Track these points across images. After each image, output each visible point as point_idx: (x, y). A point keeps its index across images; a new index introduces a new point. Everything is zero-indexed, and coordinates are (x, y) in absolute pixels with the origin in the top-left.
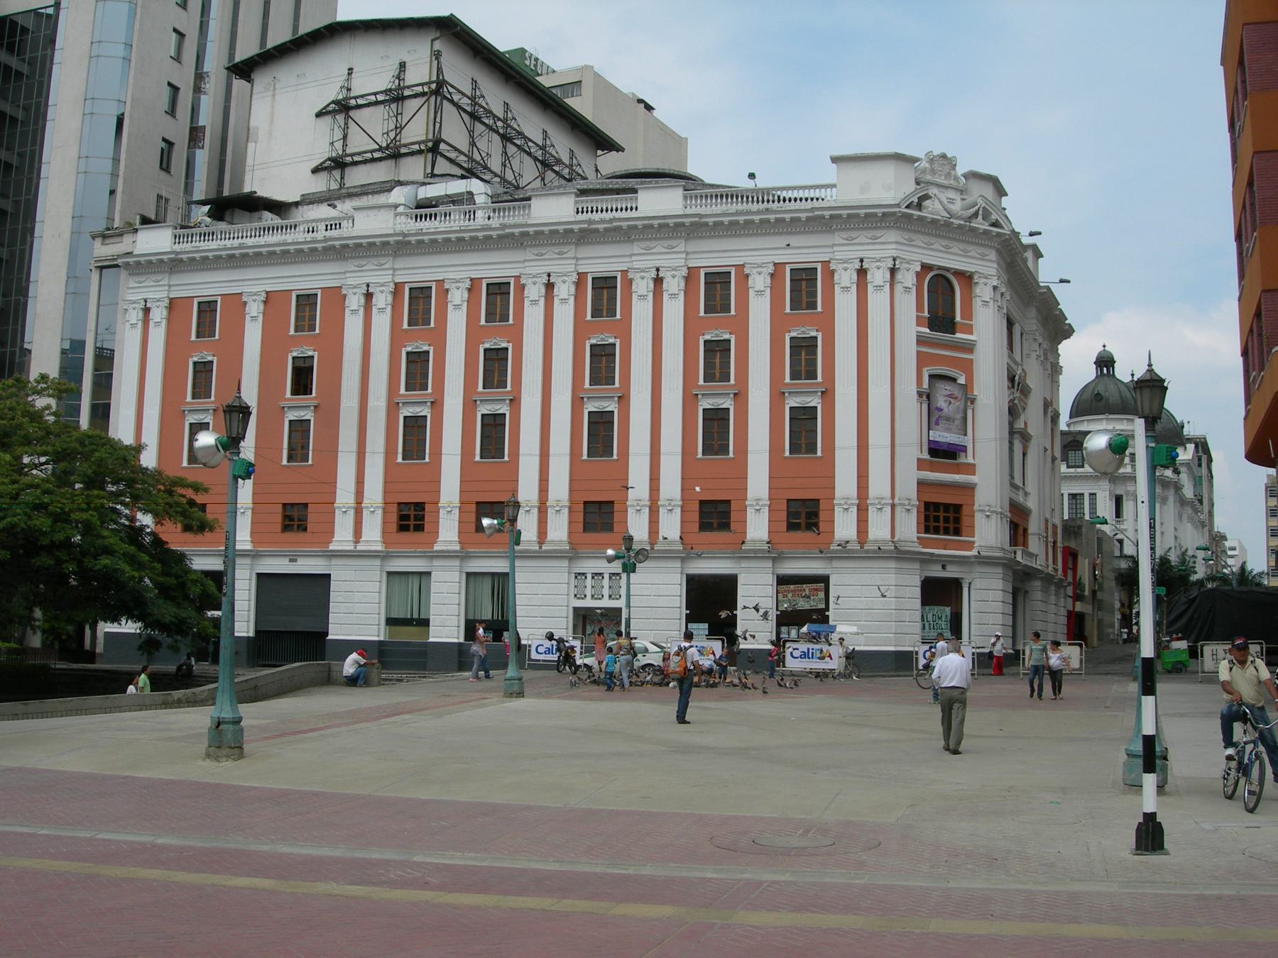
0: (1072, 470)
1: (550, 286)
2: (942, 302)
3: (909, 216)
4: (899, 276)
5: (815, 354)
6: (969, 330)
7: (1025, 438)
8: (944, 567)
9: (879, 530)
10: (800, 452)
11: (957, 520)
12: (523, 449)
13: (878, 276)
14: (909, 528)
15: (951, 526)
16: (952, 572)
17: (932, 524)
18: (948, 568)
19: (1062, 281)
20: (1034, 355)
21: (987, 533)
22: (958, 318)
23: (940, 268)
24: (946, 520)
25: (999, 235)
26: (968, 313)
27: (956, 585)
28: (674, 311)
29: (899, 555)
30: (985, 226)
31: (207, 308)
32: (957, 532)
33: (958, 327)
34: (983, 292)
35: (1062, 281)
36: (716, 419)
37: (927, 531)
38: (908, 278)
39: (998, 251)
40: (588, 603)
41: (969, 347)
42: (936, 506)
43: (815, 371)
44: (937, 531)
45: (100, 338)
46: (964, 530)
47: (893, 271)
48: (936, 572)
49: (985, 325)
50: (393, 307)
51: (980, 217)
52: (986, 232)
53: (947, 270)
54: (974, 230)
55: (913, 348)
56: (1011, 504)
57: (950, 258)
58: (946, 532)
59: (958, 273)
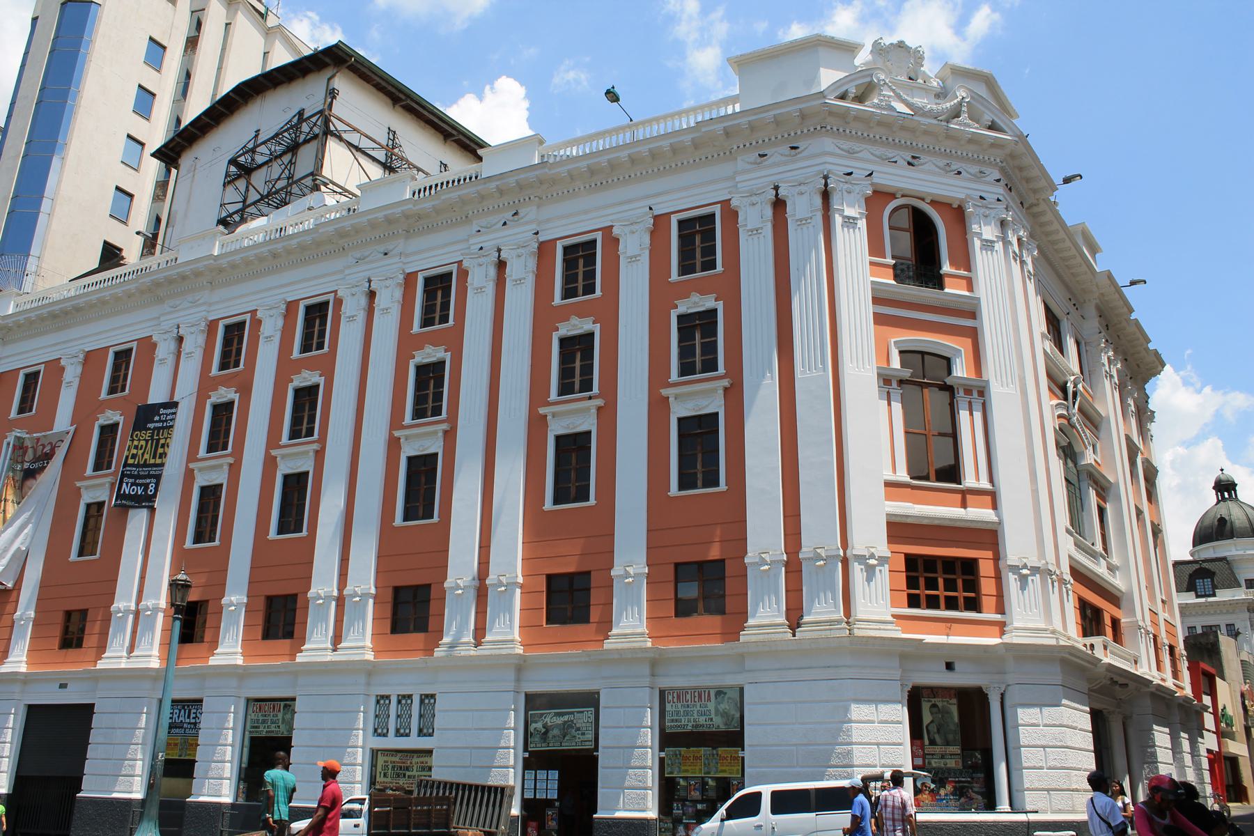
0: (1202, 600)
1: (779, 205)
2: (922, 248)
3: (843, 115)
5: (715, 334)
7: (1104, 490)
8: (949, 666)
10: (694, 486)
13: (802, 206)
17: (923, 592)
19: (1133, 283)
21: (1037, 616)
25: (996, 145)
28: (520, 301)
30: (975, 129)
31: (122, 357)
35: (1133, 283)
36: (573, 448)
37: (913, 602)
40: (392, 742)
42: (930, 563)
43: (716, 359)
44: (933, 603)
45: (667, 770)
47: (826, 195)
50: (537, 276)
51: (964, 116)
52: (974, 140)
54: (950, 136)
55: (867, 309)
57: (928, 182)
58: (952, 604)
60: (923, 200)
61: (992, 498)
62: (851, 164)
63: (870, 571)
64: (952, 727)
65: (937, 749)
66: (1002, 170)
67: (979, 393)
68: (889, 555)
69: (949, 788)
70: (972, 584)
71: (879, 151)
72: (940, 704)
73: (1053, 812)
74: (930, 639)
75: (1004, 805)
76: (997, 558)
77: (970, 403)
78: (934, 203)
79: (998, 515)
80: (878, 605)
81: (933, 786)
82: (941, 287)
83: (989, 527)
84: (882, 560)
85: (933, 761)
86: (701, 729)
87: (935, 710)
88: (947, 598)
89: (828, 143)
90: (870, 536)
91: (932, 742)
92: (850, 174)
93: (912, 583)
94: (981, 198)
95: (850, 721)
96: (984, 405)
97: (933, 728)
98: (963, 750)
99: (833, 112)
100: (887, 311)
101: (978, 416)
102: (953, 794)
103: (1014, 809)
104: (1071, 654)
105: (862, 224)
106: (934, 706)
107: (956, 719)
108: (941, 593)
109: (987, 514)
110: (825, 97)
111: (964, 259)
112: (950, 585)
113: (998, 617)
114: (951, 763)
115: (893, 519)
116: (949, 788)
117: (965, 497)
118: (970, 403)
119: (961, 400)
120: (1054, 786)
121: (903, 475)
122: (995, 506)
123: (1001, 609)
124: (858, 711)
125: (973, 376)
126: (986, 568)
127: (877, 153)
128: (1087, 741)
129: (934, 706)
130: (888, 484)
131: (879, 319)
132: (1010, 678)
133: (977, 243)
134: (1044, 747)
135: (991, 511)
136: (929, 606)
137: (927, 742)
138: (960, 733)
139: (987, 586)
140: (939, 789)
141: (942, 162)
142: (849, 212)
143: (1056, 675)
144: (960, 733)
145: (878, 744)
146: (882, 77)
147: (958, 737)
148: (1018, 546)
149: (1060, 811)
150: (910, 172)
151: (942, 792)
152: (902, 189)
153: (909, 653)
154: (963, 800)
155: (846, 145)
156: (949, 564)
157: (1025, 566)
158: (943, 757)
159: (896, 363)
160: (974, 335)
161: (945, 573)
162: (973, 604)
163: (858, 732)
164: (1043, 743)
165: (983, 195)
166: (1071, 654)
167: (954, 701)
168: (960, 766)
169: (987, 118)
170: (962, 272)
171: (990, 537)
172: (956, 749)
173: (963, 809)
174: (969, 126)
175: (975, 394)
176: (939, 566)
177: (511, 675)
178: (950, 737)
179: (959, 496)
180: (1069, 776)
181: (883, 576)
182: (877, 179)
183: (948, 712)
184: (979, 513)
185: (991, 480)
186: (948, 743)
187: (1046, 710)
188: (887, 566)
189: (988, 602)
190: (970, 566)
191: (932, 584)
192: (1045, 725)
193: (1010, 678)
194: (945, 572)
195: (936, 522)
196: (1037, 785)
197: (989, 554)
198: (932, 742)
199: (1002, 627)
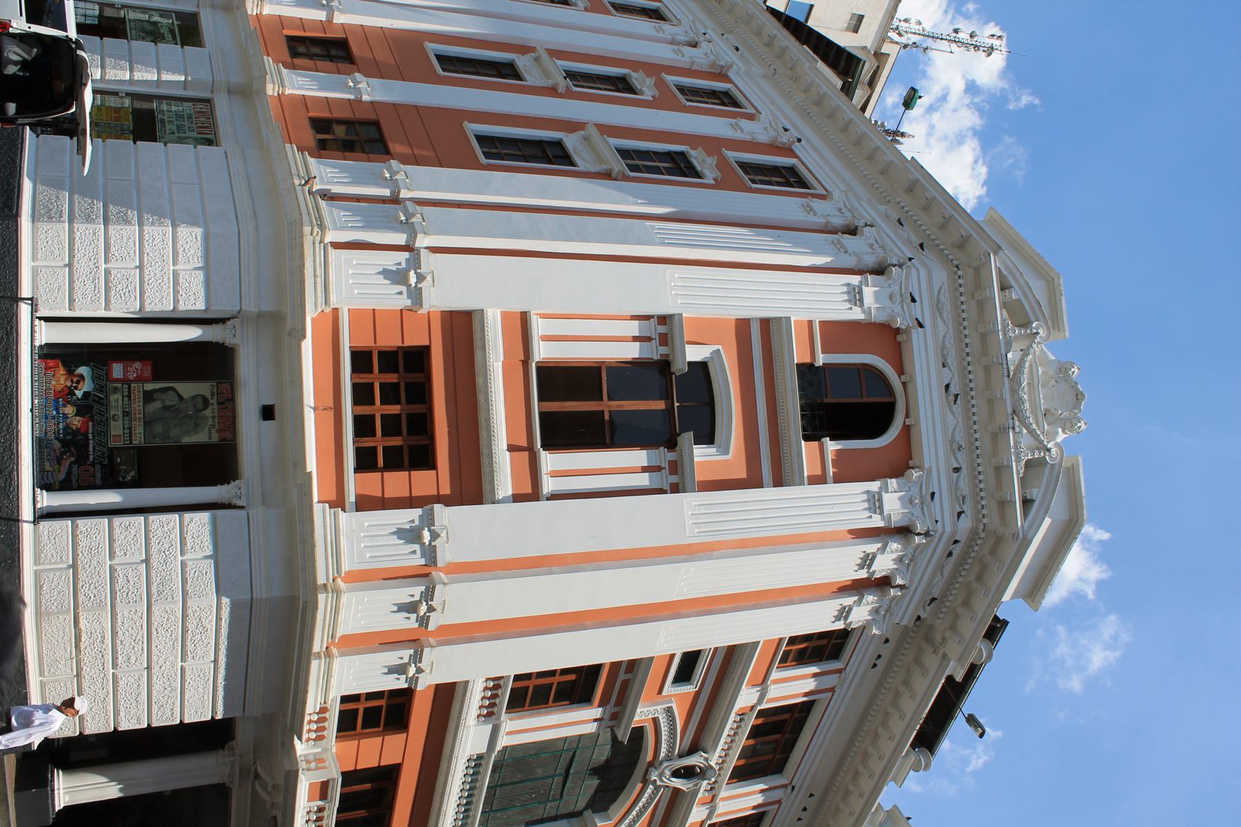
3: (983, 306)
25: (1004, 505)
37: (361, 359)
44: (362, 394)
52: (1001, 470)
58: (363, 426)
60: (907, 416)
61: (531, 493)
62: (924, 297)
63: (397, 277)
64: (175, 432)
65: (137, 405)
66: (974, 534)
67: (676, 480)
68: (423, 311)
69: (76, 422)
70: (395, 462)
71: (950, 343)
72: (208, 412)
73: (37, 575)
74: (307, 347)
75: (47, 500)
76: (439, 499)
77: (649, 339)
78: (907, 429)
79: (504, 501)
80: (349, 286)
81: (79, 394)
82: (807, 438)
83: (486, 487)
84: (416, 295)
85: (118, 396)
86: (158, 126)
87: (200, 405)
88: (374, 450)
89: (941, 276)
90: (449, 286)
91: (149, 397)
92: (913, 300)
93: (390, 359)
94: (933, 494)
95: (174, 226)
96: (661, 491)
97: (170, 400)
98: (138, 448)
99: (980, 270)
100: (758, 337)
101: (643, 480)
102: (67, 427)
103: (43, 516)
104: (305, 603)
105: (857, 314)
106: (206, 402)
107: (187, 440)
108: (379, 409)
109: (505, 484)
110: (995, 253)
111: (848, 472)
112: (391, 427)
113: (351, 497)
114: (116, 428)
115: (476, 318)
116: (76, 422)
117: (523, 450)
118: (649, 339)
119: (662, 456)
120: (82, 575)
121: (543, 352)
122: (517, 498)
123: (364, 504)
124: (191, 238)
125: (698, 477)
126: (423, 482)
127: (947, 342)
128: (165, 717)
129: (206, 402)
130: (524, 318)
131: (743, 326)
132: (257, 513)
133: (874, 486)
134: (147, 561)
135: (510, 493)
136: (358, 420)
137: (149, 386)
138: (158, 423)
139: (396, 482)
140: (74, 404)
141: (960, 438)
142: (869, 293)
143: (268, 588)
144: (158, 423)
145: (141, 267)
146: (1041, 331)
147: (158, 442)
148: (463, 530)
149: (38, 587)
150: (937, 391)
151: (70, 410)
152: (913, 379)
153: (281, 325)
154: (57, 445)
155: (945, 298)
156: (422, 424)
157: (435, 536)
158: (126, 414)
159: (694, 354)
160: (753, 481)
161: (408, 408)
162: (365, 462)
163: (158, 234)
164: (154, 562)
165: (936, 496)
166: (305, 603)
167: (215, 438)
168: (112, 444)
169: (1035, 493)
170: (831, 470)
171: (471, 488)
172: (139, 438)
173: (40, 445)
174: (1018, 461)
175: (673, 479)
176: (417, 408)
177: (236, 79)
178: (158, 428)
179: (528, 489)
180: (101, 605)
181: (392, 298)
182: (917, 334)
183: (197, 427)
184: (504, 472)
185: (555, 497)
186: (148, 423)
187: (209, 566)
188: (408, 302)
189: (372, 483)
190: (423, 458)
191: (390, 394)
192: (183, 565)
193: (257, 513)
194: (412, 449)
195: (481, 398)
196: (83, 543)
197: (446, 490)
198: (149, 397)
199: (338, 503)
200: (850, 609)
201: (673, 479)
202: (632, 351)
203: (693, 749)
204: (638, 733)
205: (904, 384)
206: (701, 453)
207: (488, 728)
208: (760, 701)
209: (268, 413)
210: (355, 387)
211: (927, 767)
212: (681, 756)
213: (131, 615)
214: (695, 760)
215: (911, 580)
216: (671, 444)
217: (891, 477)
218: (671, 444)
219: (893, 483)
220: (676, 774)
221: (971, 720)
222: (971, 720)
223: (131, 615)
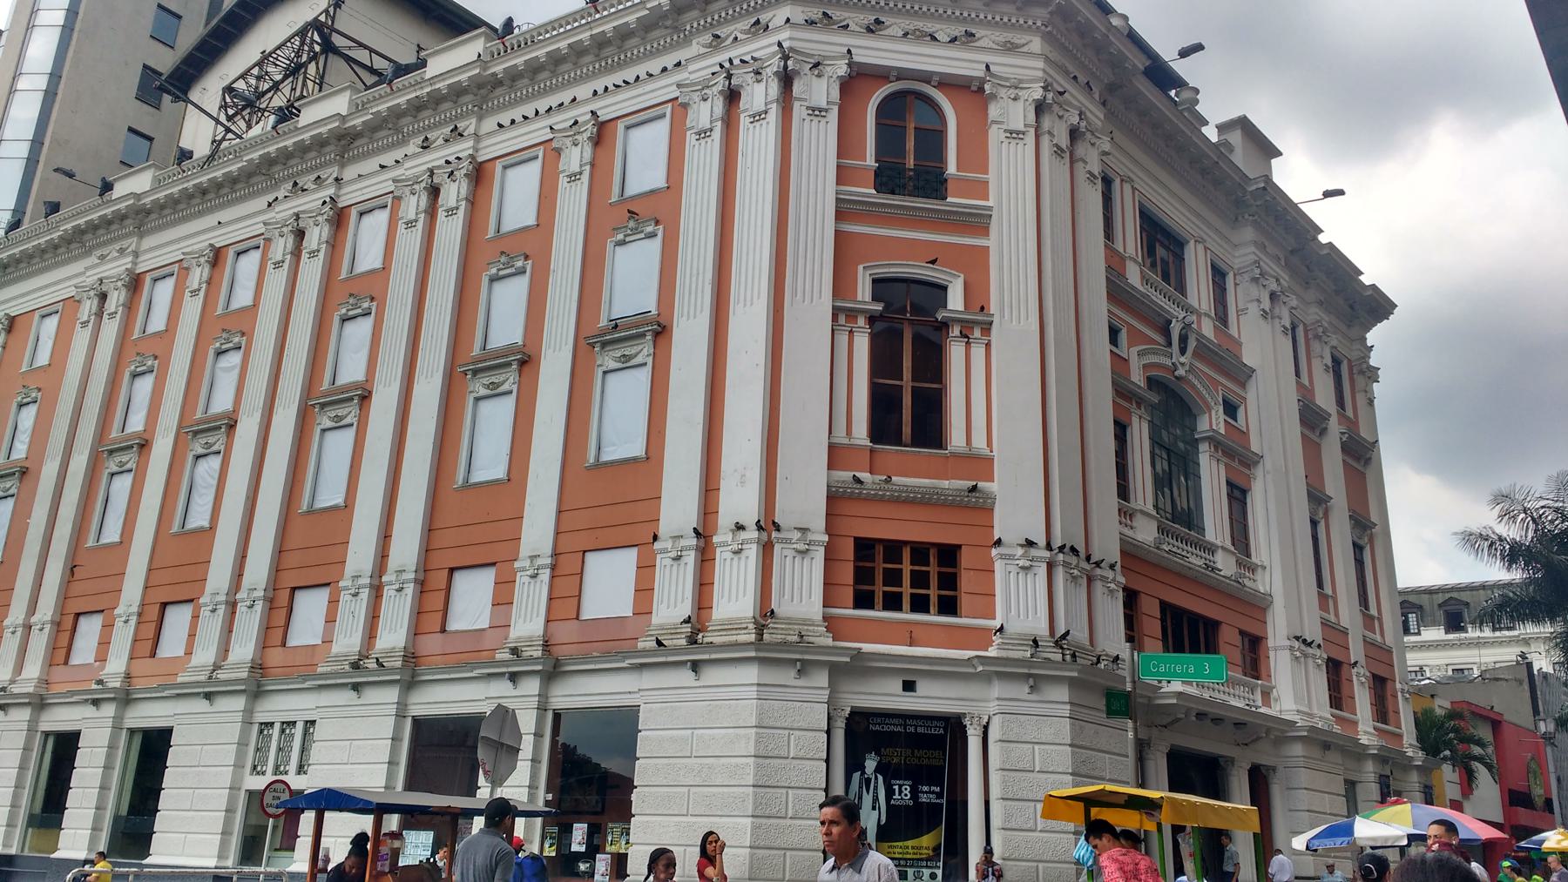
4: (797, 88)
6: (981, 189)
8: (909, 686)
9: (734, 600)
10: (871, 606)
11: (949, 581)
12: (69, 527)
13: (759, 94)
14: (803, 591)
15: (933, 593)
16: (932, 698)
18: (923, 687)
19: (1328, 194)
20: (1253, 309)
22: (952, 168)
23: (903, 74)
24: (920, 580)
26: (976, 155)
27: (951, 730)
29: (770, 645)
32: (949, 606)
33: (950, 185)
34: (1011, 112)
35: (1328, 194)
38: (820, 90)
39: (1048, 38)
41: (978, 223)
46: (965, 602)
47: (786, 79)
48: (885, 696)
49: (1016, 182)
53: (925, 77)
56: (1124, 553)
59: (949, 84)
60: (928, 82)
96: (988, 345)
138: (908, 770)
200: (1090, 173)
201: (977, 333)
202: (862, 343)
203: (1165, 331)
204: (1152, 382)
205: (898, 79)
206: (955, 300)
207: (1139, 516)
208: (1135, 261)
209: (909, 686)
210: (886, 608)
211: (1197, 91)
212: (1170, 344)
213: (740, 500)
214: (1175, 329)
215: (1075, 107)
216: (944, 326)
217: (987, 115)
218: (944, 326)
219: (994, 111)
220: (1183, 351)
221: (1184, 53)
222: (1184, 53)
223: (740, 500)
